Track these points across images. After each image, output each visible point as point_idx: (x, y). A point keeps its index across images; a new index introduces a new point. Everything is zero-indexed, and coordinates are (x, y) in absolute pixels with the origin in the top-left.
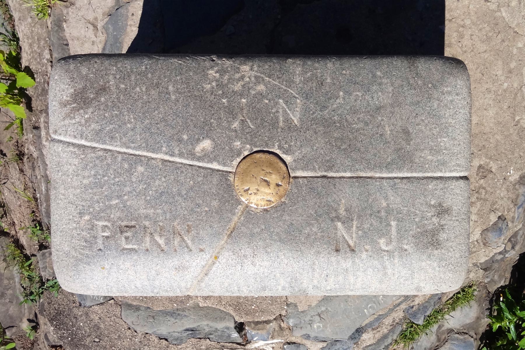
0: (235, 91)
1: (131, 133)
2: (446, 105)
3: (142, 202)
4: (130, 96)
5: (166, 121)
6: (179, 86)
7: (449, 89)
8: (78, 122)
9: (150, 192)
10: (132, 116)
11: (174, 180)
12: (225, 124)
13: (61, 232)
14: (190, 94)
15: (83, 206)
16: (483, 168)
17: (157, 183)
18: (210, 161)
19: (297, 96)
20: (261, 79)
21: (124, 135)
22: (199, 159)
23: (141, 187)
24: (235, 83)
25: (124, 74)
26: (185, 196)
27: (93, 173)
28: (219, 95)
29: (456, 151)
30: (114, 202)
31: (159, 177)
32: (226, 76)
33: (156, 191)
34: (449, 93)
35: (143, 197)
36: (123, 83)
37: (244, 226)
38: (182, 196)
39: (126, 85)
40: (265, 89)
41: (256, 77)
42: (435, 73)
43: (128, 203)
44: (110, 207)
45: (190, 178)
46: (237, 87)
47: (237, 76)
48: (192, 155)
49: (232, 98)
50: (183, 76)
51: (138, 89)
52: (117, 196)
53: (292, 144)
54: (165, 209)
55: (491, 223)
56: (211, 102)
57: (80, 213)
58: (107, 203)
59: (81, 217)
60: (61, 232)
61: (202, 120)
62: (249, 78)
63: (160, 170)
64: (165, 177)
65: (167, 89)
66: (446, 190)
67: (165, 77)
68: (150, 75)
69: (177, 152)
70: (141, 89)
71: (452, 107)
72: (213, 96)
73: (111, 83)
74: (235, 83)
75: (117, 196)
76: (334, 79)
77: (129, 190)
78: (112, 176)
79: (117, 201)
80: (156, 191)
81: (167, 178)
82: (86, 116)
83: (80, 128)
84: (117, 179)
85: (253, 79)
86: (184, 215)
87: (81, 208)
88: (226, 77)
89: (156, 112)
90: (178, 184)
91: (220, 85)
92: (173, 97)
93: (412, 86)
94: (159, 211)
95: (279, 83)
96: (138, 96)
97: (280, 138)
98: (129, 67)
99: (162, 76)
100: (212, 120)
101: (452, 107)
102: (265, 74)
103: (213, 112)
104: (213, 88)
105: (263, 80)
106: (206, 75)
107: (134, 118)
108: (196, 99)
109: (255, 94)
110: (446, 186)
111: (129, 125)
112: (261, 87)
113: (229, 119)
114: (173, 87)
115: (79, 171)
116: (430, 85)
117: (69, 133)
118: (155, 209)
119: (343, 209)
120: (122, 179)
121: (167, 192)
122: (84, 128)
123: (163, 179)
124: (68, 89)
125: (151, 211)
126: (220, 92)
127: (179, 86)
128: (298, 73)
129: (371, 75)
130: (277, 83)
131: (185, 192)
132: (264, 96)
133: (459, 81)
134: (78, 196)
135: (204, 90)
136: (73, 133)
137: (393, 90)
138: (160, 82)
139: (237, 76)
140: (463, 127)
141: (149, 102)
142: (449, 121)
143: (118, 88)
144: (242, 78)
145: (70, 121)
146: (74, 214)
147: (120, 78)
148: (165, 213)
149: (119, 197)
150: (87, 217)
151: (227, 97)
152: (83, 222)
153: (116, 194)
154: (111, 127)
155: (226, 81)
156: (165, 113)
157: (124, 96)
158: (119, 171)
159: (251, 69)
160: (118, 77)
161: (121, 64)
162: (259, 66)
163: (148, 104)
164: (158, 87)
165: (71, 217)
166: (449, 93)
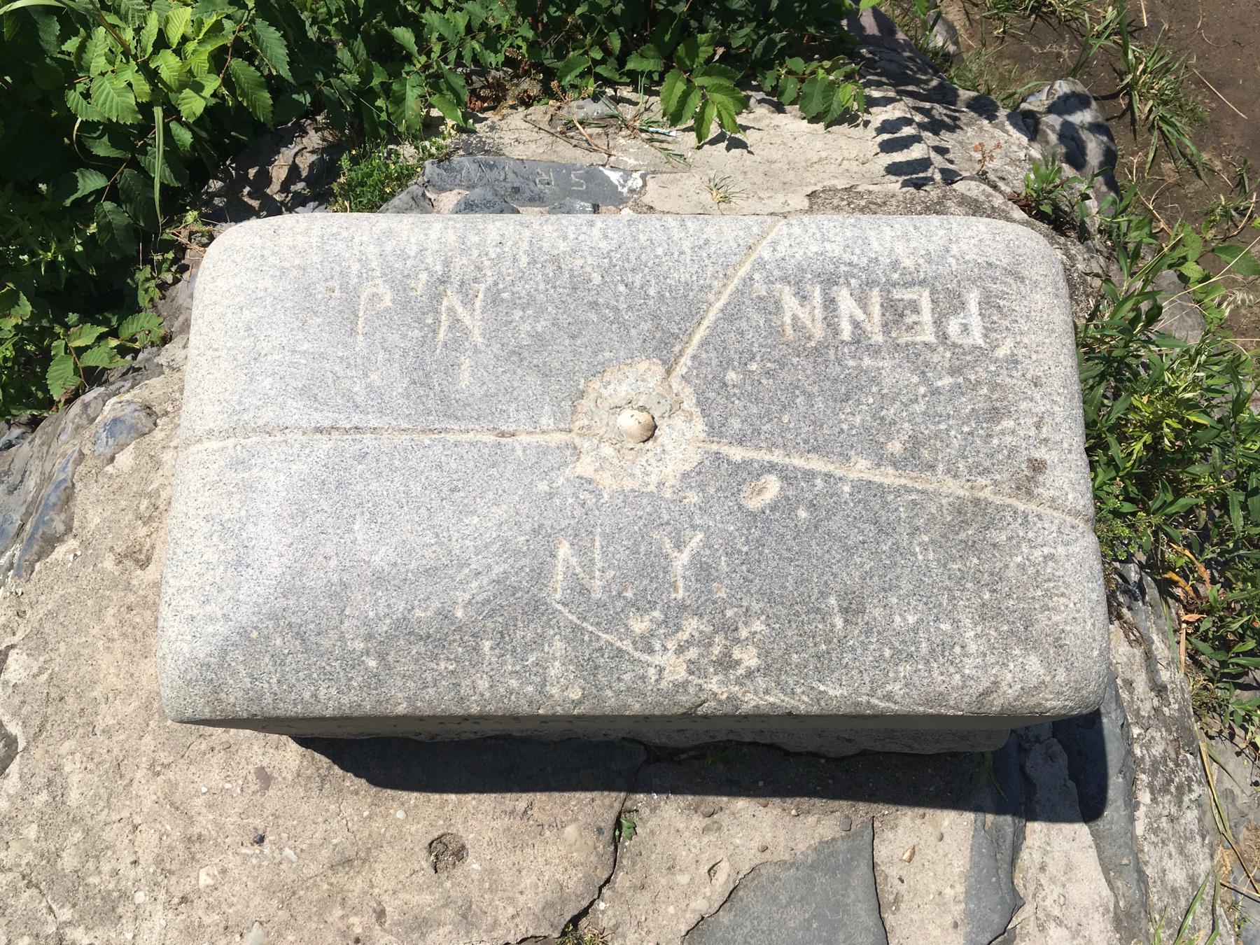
0: (696, 618)
1: (920, 522)
2: (220, 590)
3: (887, 382)
4: (926, 604)
5: (846, 549)
6: (820, 626)
7: (210, 629)
8: (1035, 547)
9: (871, 401)
10: (920, 557)
11: (821, 426)
12: (717, 543)
13: (1053, 331)
14: (796, 607)
15: (1011, 376)
16: (137, 561)
17: (858, 419)
18: (746, 464)
19: (559, 607)
20: (640, 646)
21: (935, 518)
22: (771, 468)
23: (892, 411)
24: (697, 635)
25: (944, 657)
26: (797, 392)
27: (995, 441)
28: (732, 606)
29: (207, 494)
30: (947, 381)
31: (854, 432)
32: (716, 652)
33: (859, 402)
34: (211, 619)
35: (885, 391)
36: (945, 633)
37: (673, 334)
38: (804, 393)
39: (938, 629)
40: (631, 622)
41: (651, 651)
42: (241, 667)
43: (915, 379)
44: (953, 371)
45: (789, 429)
46: (692, 626)
47: (693, 653)
48: (787, 476)
49: (703, 599)
50: (812, 651)
51: (911, 619)
52: (940, 393)
53: (571, 500)
54: (839, 369)
55: (132, 446)
56: (749, 591)
57: (1017, 362)
58: (961, 380)
59: (1013, 355)
60: (1053, 331)
61: (767, 551)
62: (665, 649)
63: (852, 446)
64: (842, 430)
65: (846, 621)
66: (237, 408)
67: (853, 649)
68: (887, 653)
69: (819, 482)
70: (904, 619)
71: (207, 588)
72: (745, 604)
73: (972, 633)
74: (697, 635)
75: (940, 393)
76: (474, 649)
77: (916, 406)
78: (953, 433)
79: (939, 384)
80: (859, 402)
81: (838, 430)
82: (1019, 559)
83: (1031, 535)
84: (943, 426)
85: (658, 647)
86: (798, 356)
87: (1014, 373)
88: (716, 650)
89: (867, 567)
90: (812, 418)
91: (730, 629)
92: (832, 601)
93: (297, 633)
94: (851, 363)
95: (598, 639)
96: (909, 604)
97: (597, 513)
98: (936, 673)
99: (859, 651)
100: (745, 549)
101: (207, 588)
102: (633, 661)
103: (744, 567)
104: (746, 624)
105: (634, 643)
106: (764, 653)
107: (914, 555)
108: (781, 596)
109: (653, 608)
110: (235, 418)
111: (926, 538)
112: (639, 626)
113: (708, 552)
114: (833, 626)
115: (1024, 445)
116: (255, 634)
117: (1054, 528)
118: (858, 367)
119: (463, 367)
120: (933, 427)
121: (835, 401)
122: (1021, 534)
123: (845, 427)
124: (1066, 623)
125: (867, 362)
126: (729, 613)
127: (820, 626)
128: (557, 664)
129: (390, 659)
130: (604, 636)
131: (798, 401)
132: (633, 605)
133: (186, 648)
134: (1022, 396)
135: (763, 618)
136: (1046, 526)
137: (342, 623)
138: (863, 638)
139: (693, 653)
140: (184, 548)
141: (884, 590)
142: (216, 556)
143: (956, 622)
144: (680, 650)
145: (1053, 551)
146: (1027, 361)
147: (953, 647)
148: (839, 362)
149: (936, 392)
150: (1001, 352)
151: (714, 602)
152: (1009, 342)
153: (942, 398)
154: (962, 536)
155: (717, 640)
156: (847, 566)
157: (940, 605)
158: (939, 444)
159: (661, 670)
160: (957, 649)
161: (954, 683)
162: (643, 678)
163: (887, 586)
164: (867, 623)
165: (1034, 357)
166: (211, 619)
